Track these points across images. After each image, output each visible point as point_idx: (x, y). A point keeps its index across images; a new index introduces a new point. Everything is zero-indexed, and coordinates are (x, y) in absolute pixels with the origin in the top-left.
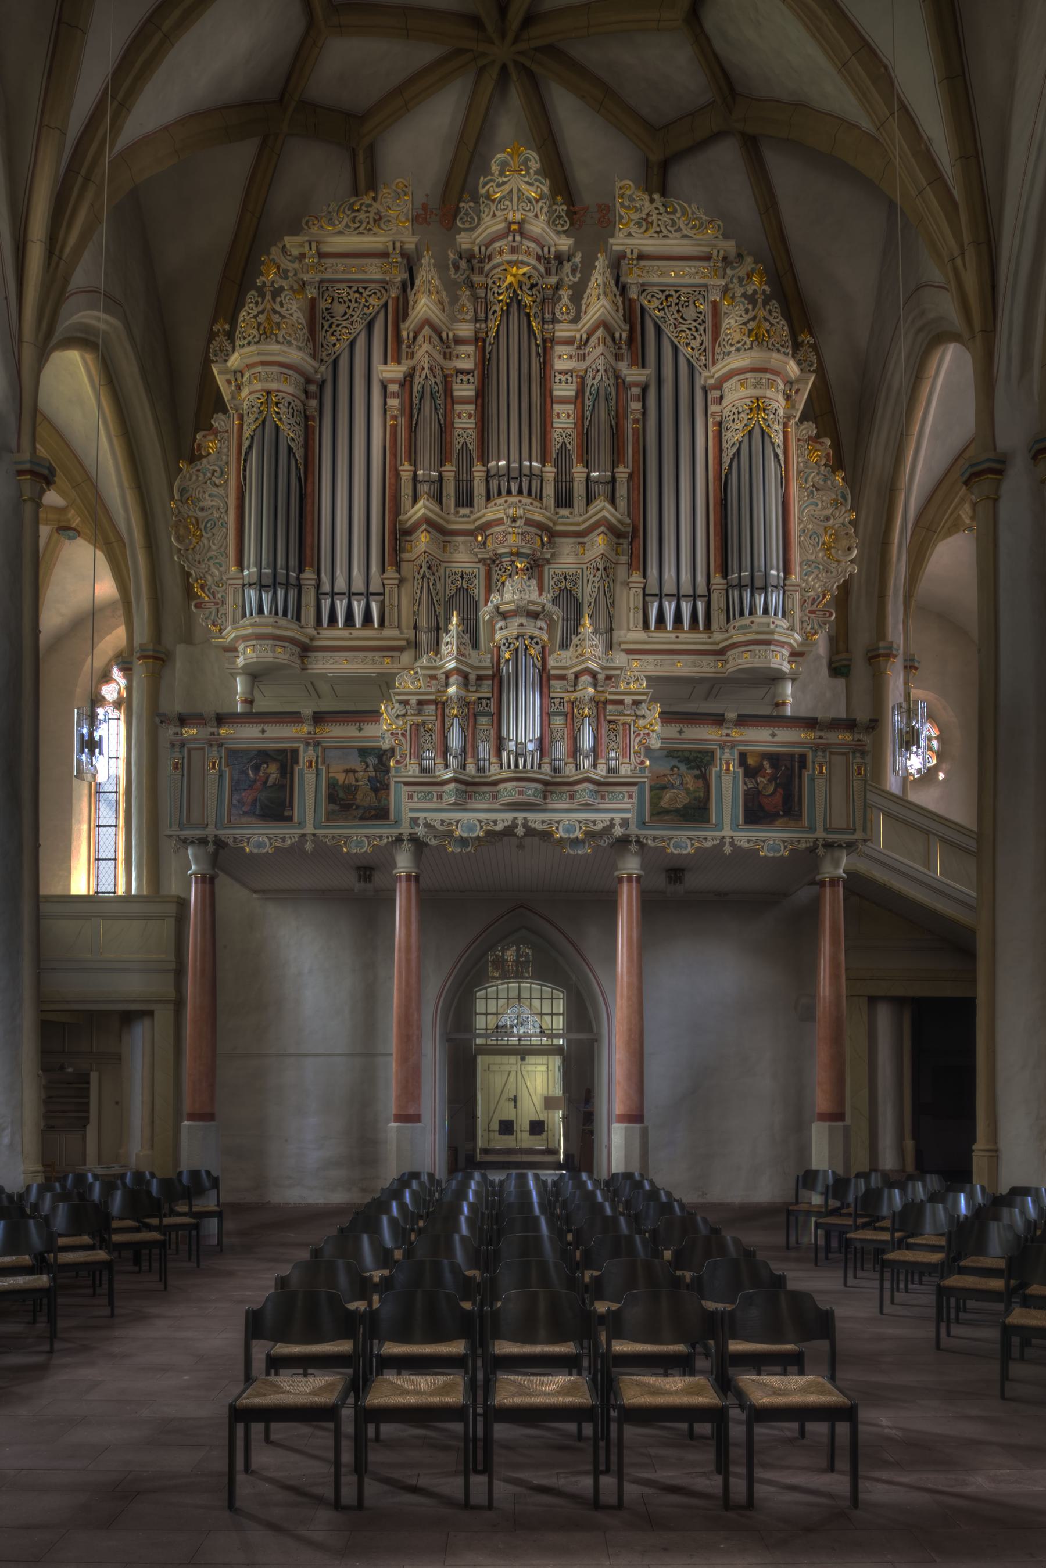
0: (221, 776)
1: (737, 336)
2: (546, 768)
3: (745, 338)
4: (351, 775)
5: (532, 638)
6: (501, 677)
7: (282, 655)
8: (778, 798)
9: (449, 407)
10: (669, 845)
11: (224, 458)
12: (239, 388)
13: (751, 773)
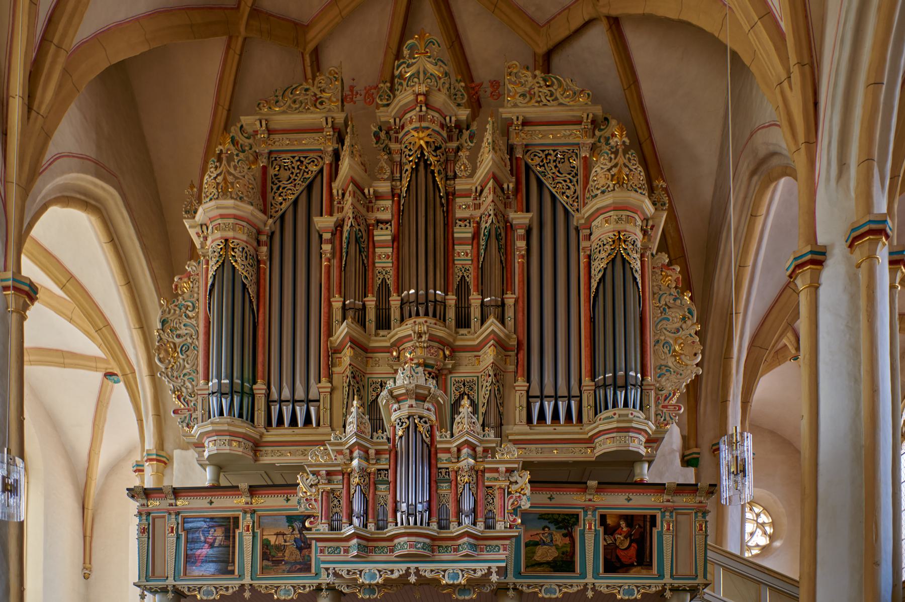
0: (178, 538)
1: (602, 181)
2: (434, 526)
3: (609, 182)
4: (280, 537)
5: (421, 418)
6: (396, 452)
7: (237, 449)
8: (633, 551)
9: (371, 250)
10: (540, 590)
11: (196, 295)
12: (206, 238)
13: (610, 531)
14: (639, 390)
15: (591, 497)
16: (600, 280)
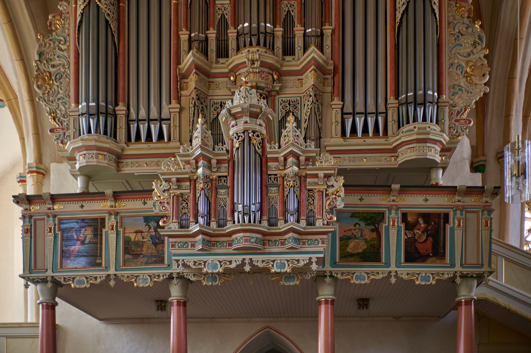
0: (55, 237)
2: (265, 223)
4: (139, 234)
5: (254, 132)
8: (429, 244)
10: (352, 277)
11: (67, 31)
13: (409, 227)
14: (436, 107)
15: (395, 198)
16: (404, 11)
